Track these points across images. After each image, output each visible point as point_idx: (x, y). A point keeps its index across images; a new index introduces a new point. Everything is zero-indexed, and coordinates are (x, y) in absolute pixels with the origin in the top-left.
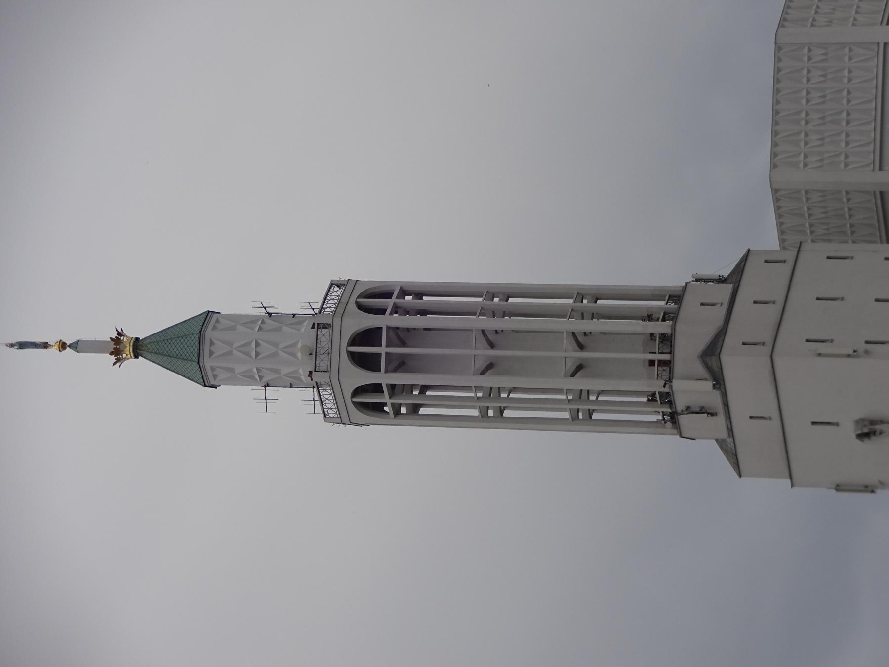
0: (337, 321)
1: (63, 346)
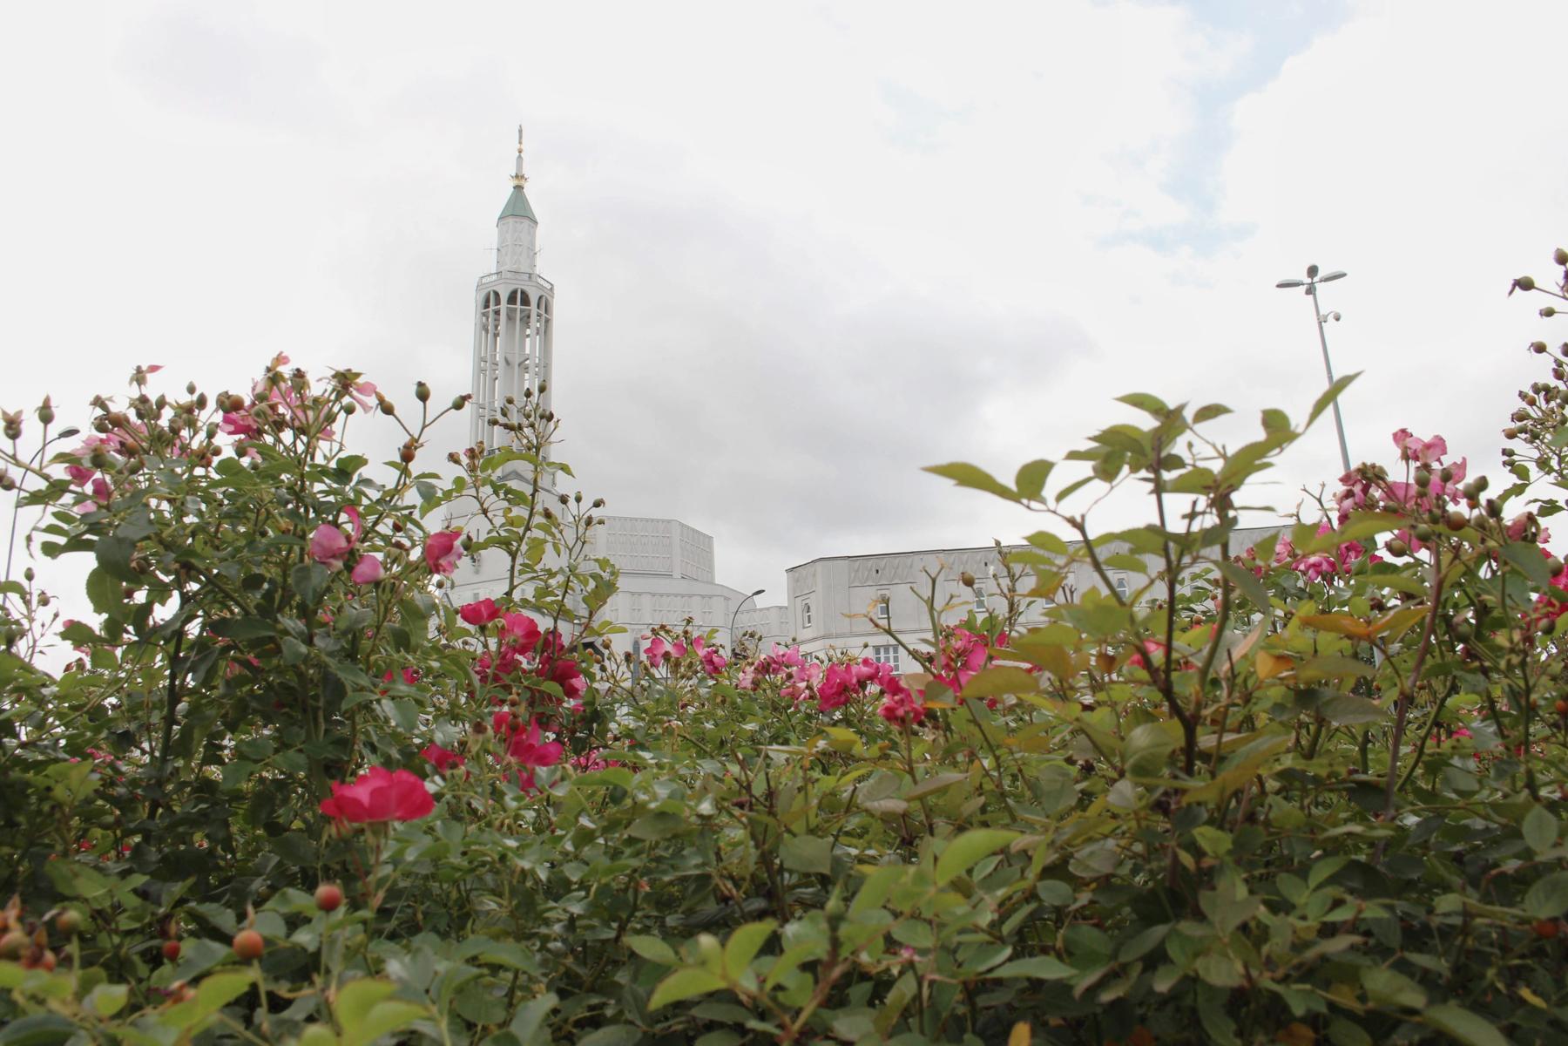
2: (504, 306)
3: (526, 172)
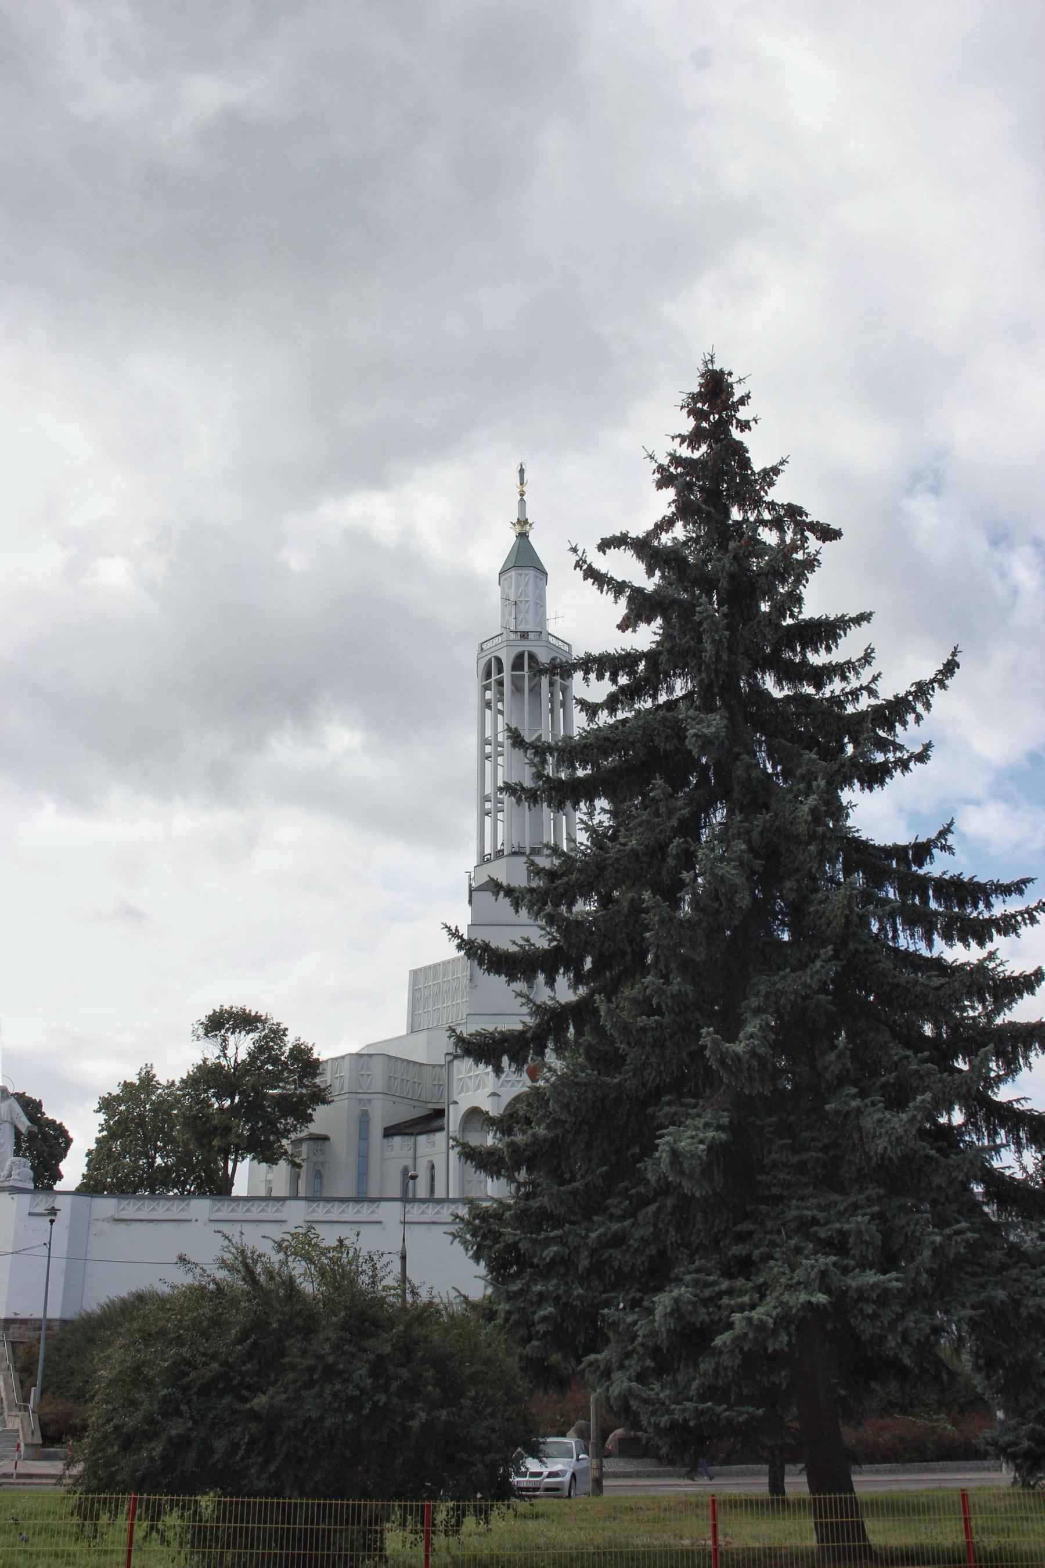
0: (544, 644)
1: (522, 495)
2: (507, 675)
3: (530, 517)
